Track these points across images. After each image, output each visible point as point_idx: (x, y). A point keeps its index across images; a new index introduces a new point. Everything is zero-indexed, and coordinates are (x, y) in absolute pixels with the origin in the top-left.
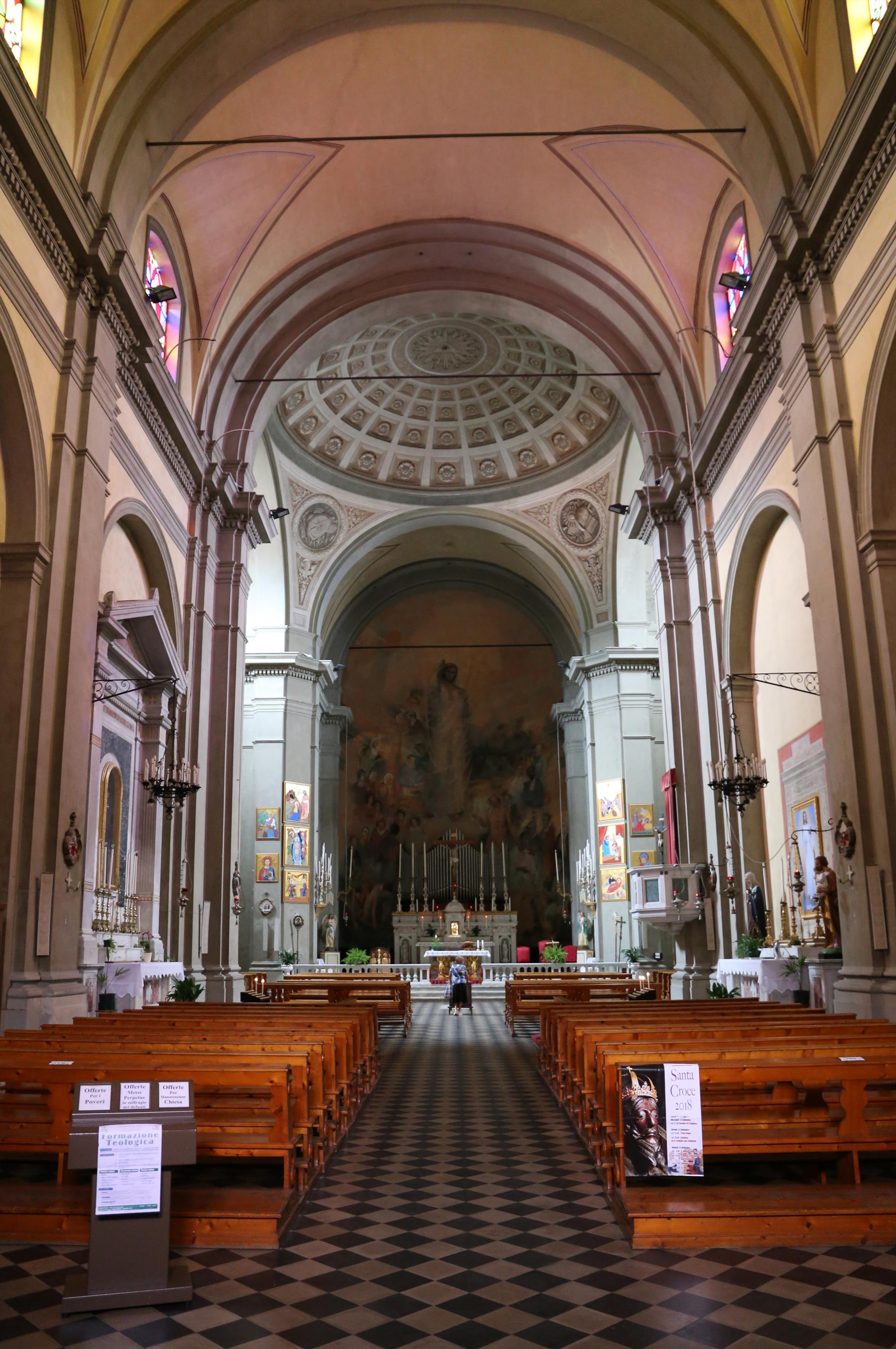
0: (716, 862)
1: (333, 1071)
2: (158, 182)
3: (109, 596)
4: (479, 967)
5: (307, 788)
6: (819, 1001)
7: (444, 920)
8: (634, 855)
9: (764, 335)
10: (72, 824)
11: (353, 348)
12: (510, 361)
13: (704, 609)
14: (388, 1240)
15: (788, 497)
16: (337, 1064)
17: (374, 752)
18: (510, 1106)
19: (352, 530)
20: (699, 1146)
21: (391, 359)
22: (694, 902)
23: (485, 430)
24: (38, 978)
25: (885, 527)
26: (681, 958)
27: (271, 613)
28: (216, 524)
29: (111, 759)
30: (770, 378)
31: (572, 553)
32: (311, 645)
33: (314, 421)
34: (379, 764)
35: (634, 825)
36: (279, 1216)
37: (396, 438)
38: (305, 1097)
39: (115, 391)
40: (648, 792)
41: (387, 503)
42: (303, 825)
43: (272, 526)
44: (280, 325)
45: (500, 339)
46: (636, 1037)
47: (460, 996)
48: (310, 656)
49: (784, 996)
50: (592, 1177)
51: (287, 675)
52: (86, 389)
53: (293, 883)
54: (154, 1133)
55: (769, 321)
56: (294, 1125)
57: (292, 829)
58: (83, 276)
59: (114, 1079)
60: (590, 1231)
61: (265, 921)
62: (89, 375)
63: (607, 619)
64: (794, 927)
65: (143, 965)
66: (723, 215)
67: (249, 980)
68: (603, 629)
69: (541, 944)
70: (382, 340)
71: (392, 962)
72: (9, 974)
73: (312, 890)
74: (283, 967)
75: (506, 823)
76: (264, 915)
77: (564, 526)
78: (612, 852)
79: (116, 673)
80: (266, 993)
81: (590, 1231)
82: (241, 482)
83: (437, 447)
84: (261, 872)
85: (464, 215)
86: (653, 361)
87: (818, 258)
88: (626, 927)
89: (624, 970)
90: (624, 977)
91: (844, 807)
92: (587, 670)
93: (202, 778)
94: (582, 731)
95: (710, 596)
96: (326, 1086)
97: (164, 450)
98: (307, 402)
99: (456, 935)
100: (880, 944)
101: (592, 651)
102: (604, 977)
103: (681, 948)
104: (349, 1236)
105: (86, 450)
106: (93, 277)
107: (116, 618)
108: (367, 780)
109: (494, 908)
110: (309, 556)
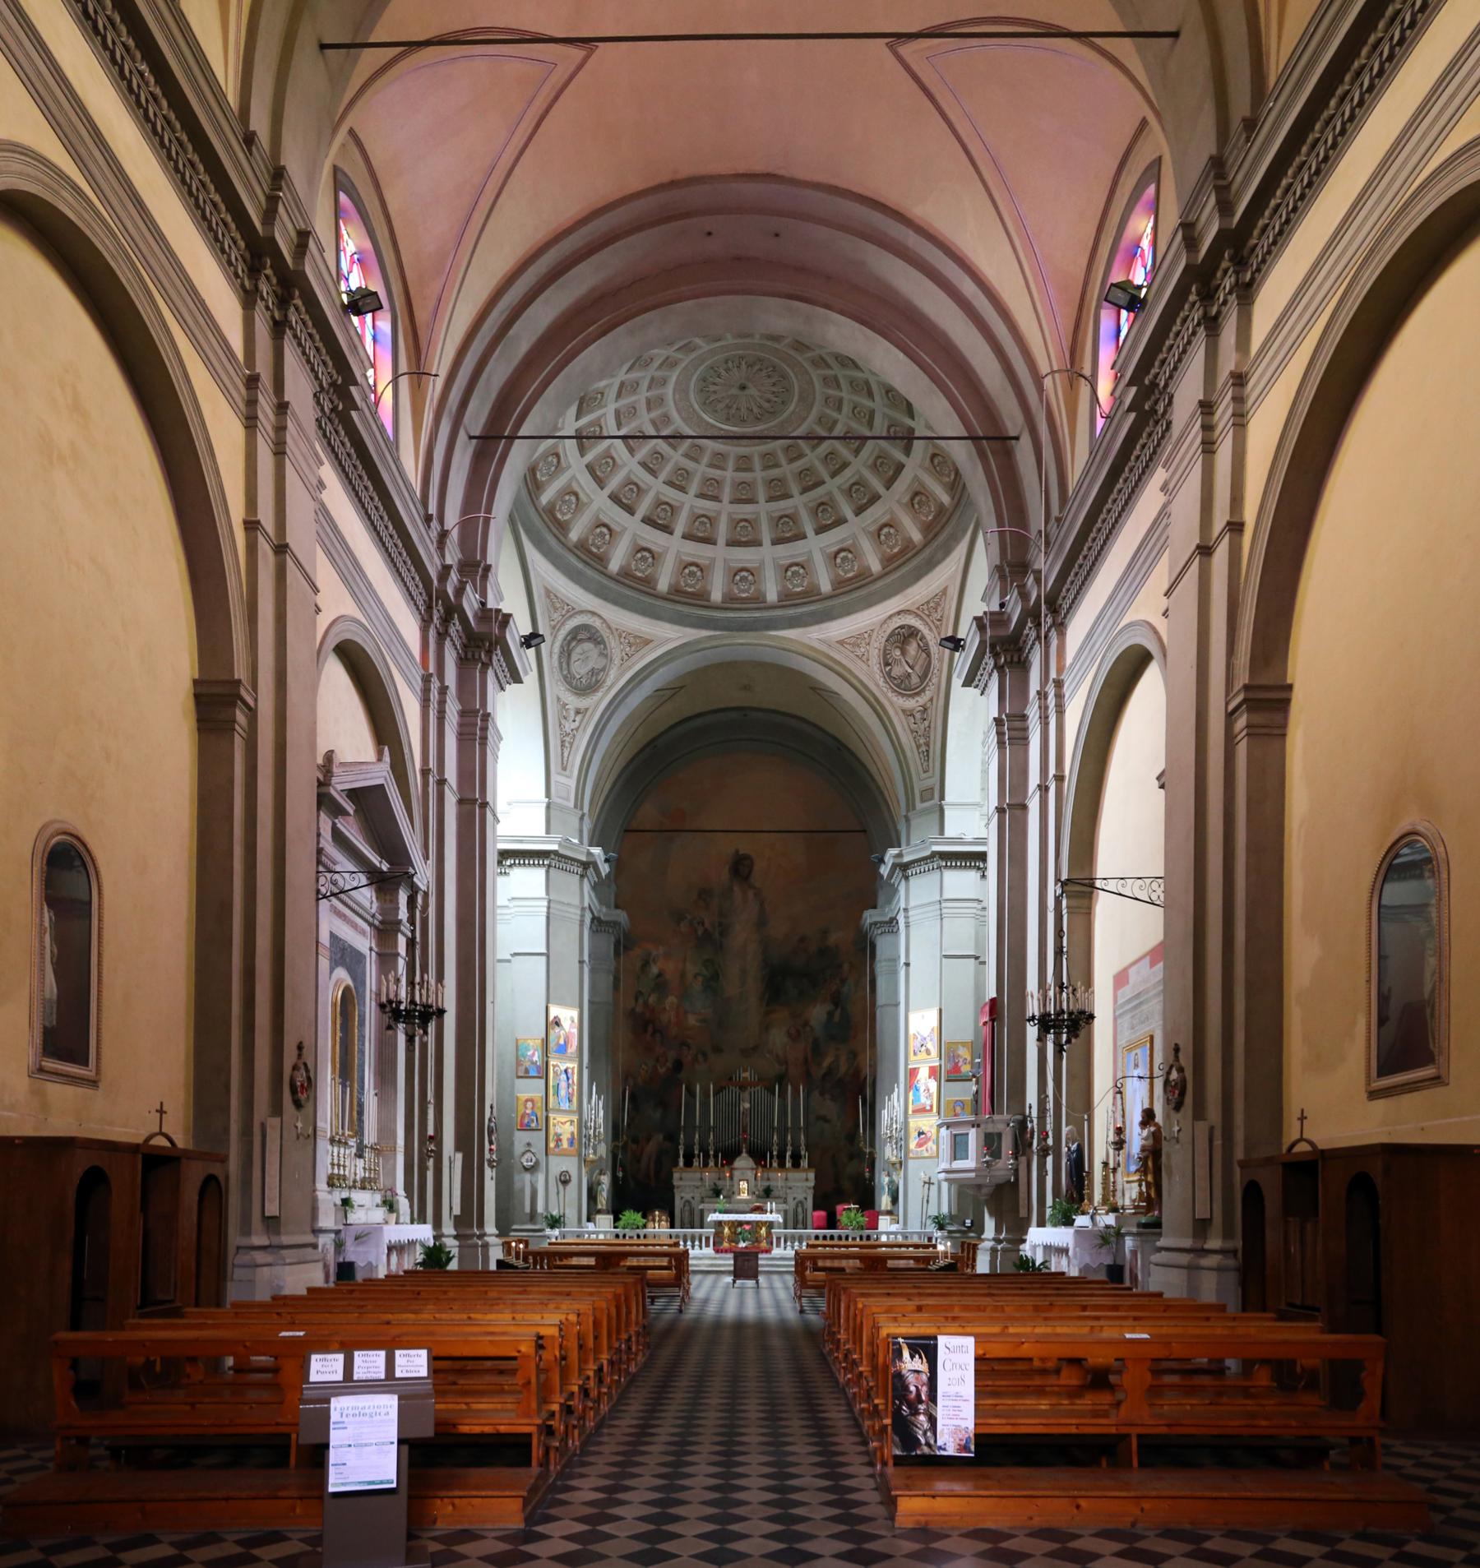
0: (1034, 1113)
1: (591, 1343)
2: (341, 110)
3: (329, 756)
4: (769, 1234)
5: (575, 1014)
6: (1134, 1278)
7: (731, 1177)
8: (948, 1102)
9: (1154, 384)
10: (300, 1056)
11: (622, 384)
12: (828, 411)
13: (1043, 788)
14: (641, 1519)
15: (1156, 632)
16: (596, 1338)
17: (655, 970)
18: (787, 1387)
19: (629, 663)
20: (970, 1424)
21: (672, 403)
22: (1007, 1161)
23: (792, 517)
24: (267, 1243)
25: (1264, 681)
26: (990, 1225)
27: (528, 785)
28: (454, 654)
29: (341, 974)
30: (1155, 452)
31: (896, 703)
32: (577, 825)
33: (573, 499)
34: (660, 985)
35: (949, 1067)
36: (525, 1494)
37: (680, 528)
38: (557, 1370)
39: (317, 454)
40: (968, 1026)
41: (667, 625)
42: (570, 1060)
43: (526, 659)
44: (524, 347)
45: (816, 375)
46: (919, 1309)
47: (746, 1267)
48: (576, 841)
49: (1095, 1271)
50: (865, 1459)
51: (549, 866)
52: (280, 452)
53: (559, 1131)
54: (388, 1405)
55: (1163, 362)
56: (544, 1400)
57: (558, 1064)
58: (259, 271)
59: (348, 1349)
60: (854, 1511)
61: (527, 1177)
62: (281, 429)
63: (932, 798)
64: (1114, 1191)
65: (385, 1227)
66: (1131, 180)
67: (506, 1246)
68: (926, 812)
69: (839, 1208)
70: (659, 373)
71: (672, 1226)
72: (234, 1238)
73: (581, 1139)
74: (548, 1232)
75: (806, 1059)
76: (526, 1169)
77: (887, 664)
78: (923, 1100)
79: (344, 863)
80: (525, 1260)
81: (854, 1511)
82: (484, 594)
83: (732, 543)
84: (523, 1117)
85: (770, 170)
86: (1012, 420)
87: (1240, 262)
88: (934, 1188)
89: (930, 1239)
90: (926, 1247)
91: (1177, 1049)
92: (905, 867)
93: (450, 1003)
94: (896, 946)
95: (1052, 771)
96: (583, 1361)
97: (384, 544)
98: (563, 470)
99: (745, 1196)
100: (1202, 1212)
101: (914, 841)
102: (908, 1246)
103: (991, 1215)
104: (599, 1515)
105: (287, 546)
106: (273, 273)
107: (340, 787)
108: (646, 1003)
109: (788, 1165)
110: (573, 702)
